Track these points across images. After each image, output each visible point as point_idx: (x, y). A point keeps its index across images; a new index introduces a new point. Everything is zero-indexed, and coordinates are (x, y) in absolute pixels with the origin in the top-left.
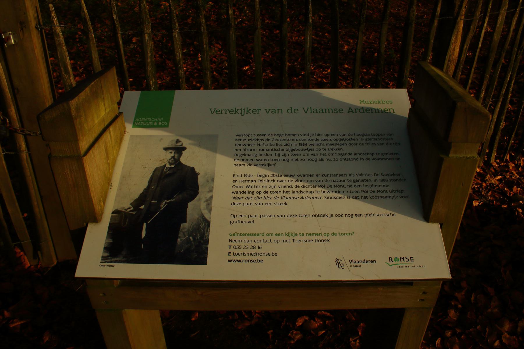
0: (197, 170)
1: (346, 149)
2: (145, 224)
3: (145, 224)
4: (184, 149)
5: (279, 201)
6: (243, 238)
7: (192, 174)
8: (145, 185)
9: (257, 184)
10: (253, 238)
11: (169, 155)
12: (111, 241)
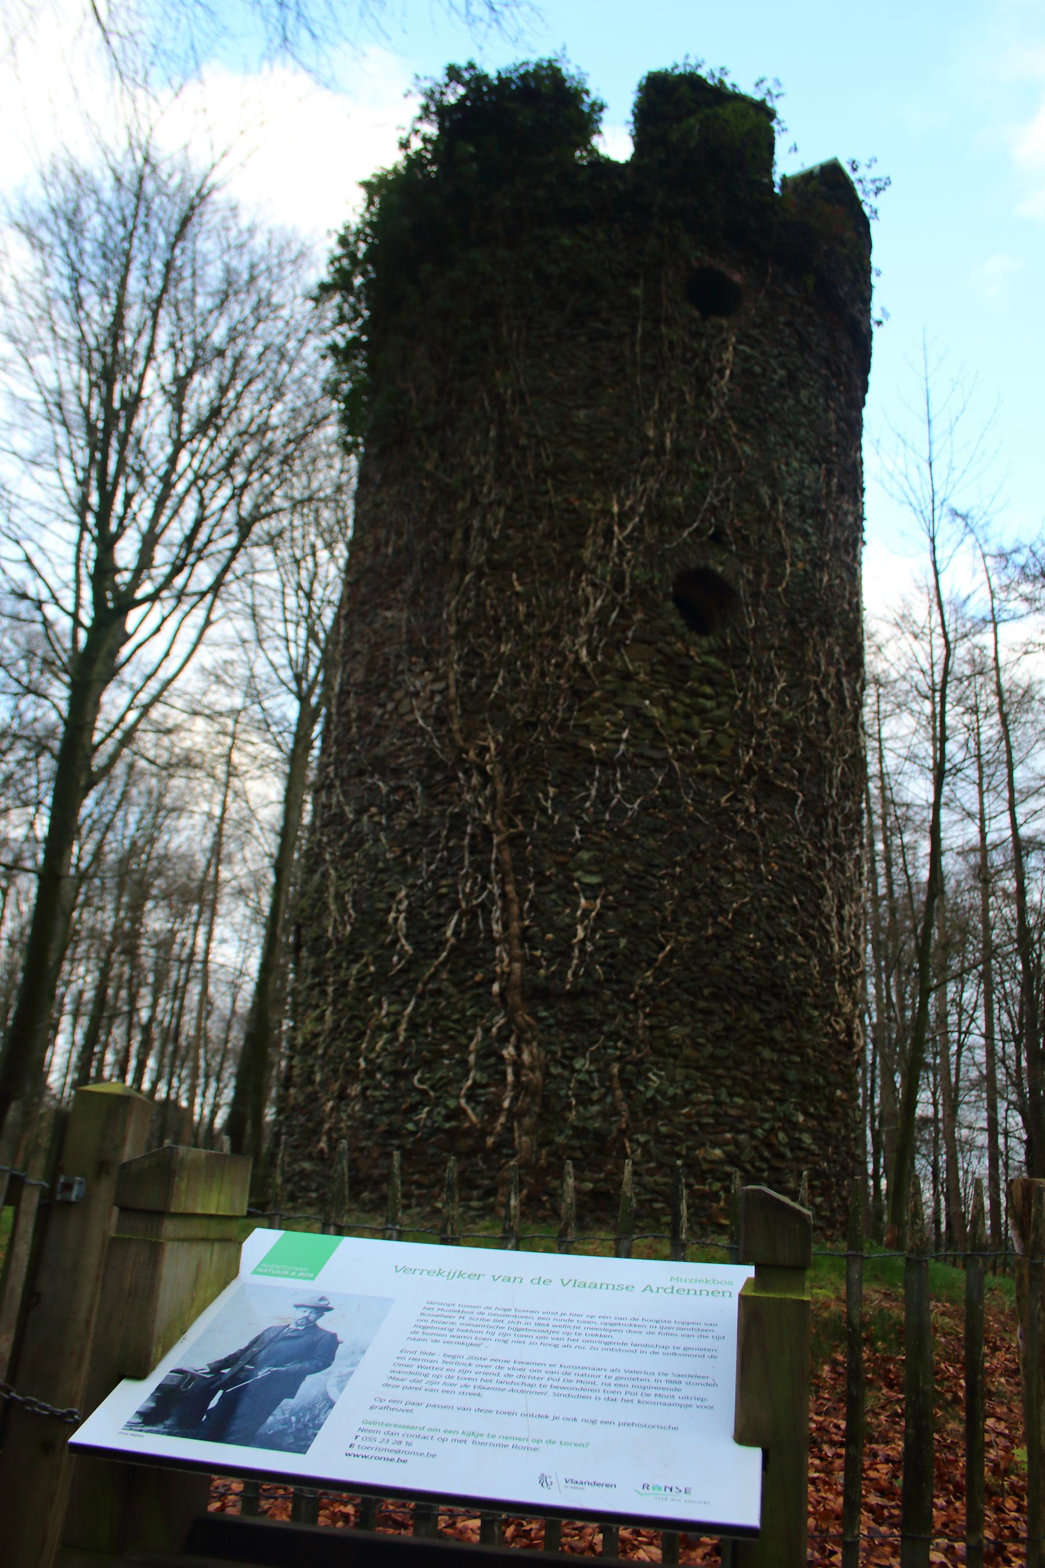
0: (340, 1338)
1: (617, 1337)
2: (220, 1393)
3: (220, 1393)
4: (330, 1309)
5: (470, 1390)
6: (383, 1429)
7: (332, 1342)
8: (243, 1345)
9: (439, 1365)
10: (402, 1431)
11: (301, 1314)
12: (153, 1405)
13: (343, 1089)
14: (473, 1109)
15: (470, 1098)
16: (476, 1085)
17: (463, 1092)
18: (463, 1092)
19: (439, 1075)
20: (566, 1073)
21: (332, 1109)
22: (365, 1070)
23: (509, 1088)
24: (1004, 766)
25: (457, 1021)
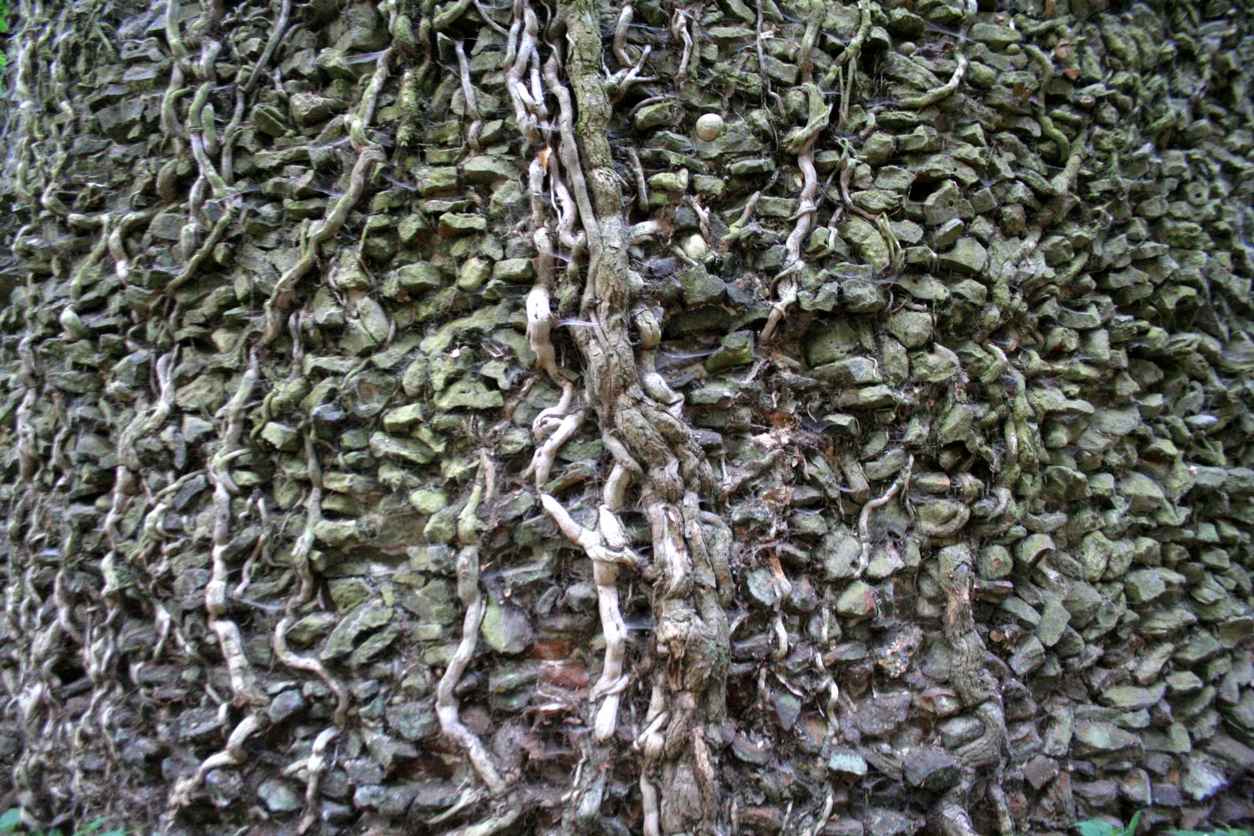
13: (68, 646)
14: (486, 739)
15: (466, 700)
16: (486, 659)
17: (446, 684)
18: (446, 684)
19: (363, 618)
20: (802, 590)
21: (41, 708)
22: (119, 595)
23: (610, 664)
24: (300, 380)
25: (404, 432)
